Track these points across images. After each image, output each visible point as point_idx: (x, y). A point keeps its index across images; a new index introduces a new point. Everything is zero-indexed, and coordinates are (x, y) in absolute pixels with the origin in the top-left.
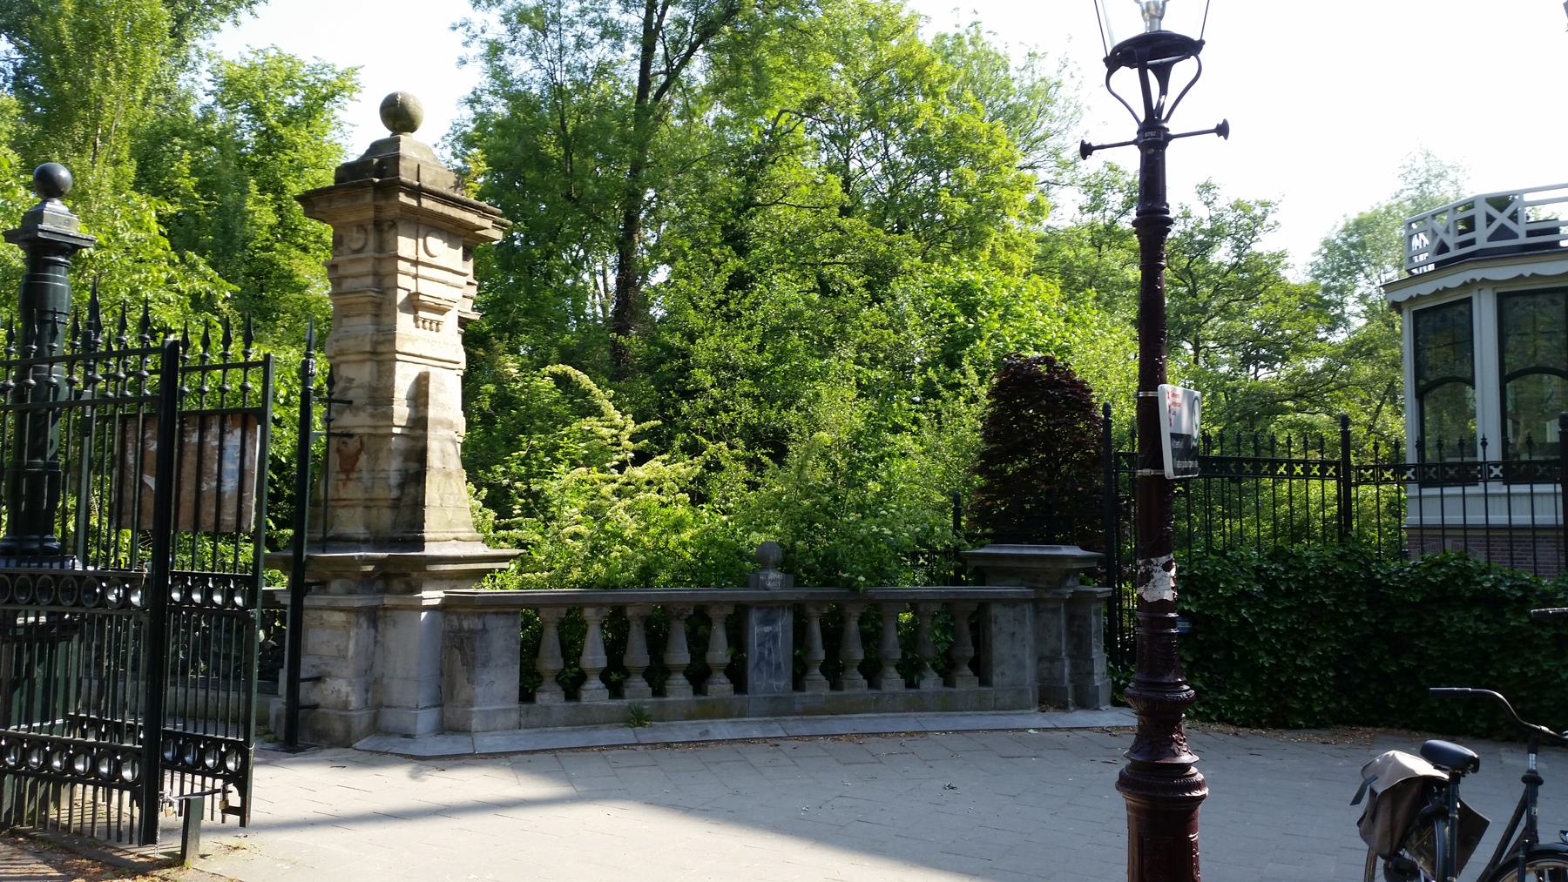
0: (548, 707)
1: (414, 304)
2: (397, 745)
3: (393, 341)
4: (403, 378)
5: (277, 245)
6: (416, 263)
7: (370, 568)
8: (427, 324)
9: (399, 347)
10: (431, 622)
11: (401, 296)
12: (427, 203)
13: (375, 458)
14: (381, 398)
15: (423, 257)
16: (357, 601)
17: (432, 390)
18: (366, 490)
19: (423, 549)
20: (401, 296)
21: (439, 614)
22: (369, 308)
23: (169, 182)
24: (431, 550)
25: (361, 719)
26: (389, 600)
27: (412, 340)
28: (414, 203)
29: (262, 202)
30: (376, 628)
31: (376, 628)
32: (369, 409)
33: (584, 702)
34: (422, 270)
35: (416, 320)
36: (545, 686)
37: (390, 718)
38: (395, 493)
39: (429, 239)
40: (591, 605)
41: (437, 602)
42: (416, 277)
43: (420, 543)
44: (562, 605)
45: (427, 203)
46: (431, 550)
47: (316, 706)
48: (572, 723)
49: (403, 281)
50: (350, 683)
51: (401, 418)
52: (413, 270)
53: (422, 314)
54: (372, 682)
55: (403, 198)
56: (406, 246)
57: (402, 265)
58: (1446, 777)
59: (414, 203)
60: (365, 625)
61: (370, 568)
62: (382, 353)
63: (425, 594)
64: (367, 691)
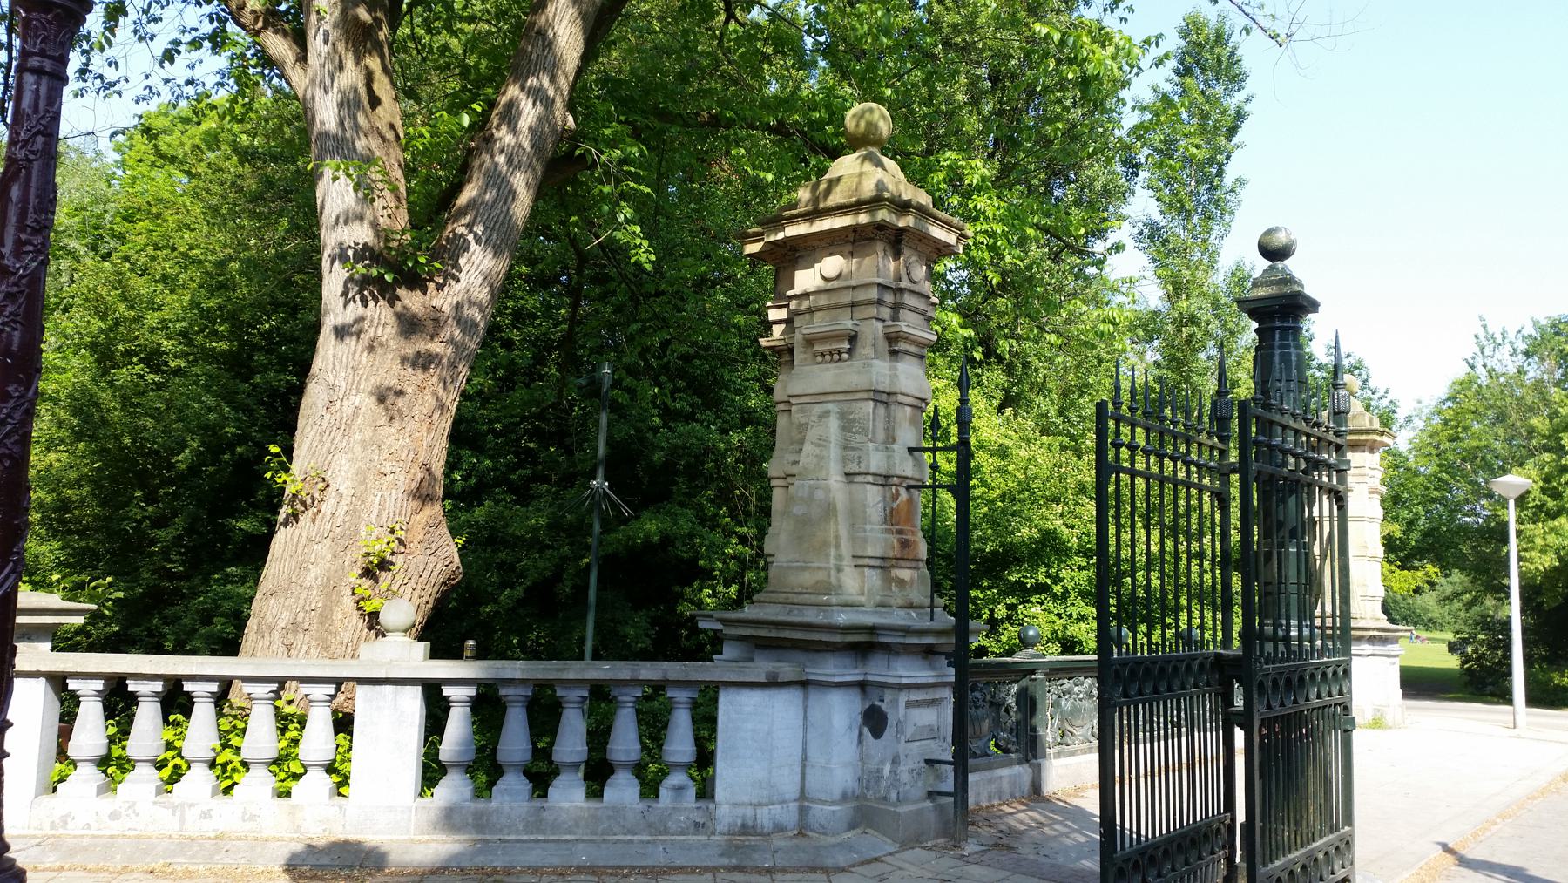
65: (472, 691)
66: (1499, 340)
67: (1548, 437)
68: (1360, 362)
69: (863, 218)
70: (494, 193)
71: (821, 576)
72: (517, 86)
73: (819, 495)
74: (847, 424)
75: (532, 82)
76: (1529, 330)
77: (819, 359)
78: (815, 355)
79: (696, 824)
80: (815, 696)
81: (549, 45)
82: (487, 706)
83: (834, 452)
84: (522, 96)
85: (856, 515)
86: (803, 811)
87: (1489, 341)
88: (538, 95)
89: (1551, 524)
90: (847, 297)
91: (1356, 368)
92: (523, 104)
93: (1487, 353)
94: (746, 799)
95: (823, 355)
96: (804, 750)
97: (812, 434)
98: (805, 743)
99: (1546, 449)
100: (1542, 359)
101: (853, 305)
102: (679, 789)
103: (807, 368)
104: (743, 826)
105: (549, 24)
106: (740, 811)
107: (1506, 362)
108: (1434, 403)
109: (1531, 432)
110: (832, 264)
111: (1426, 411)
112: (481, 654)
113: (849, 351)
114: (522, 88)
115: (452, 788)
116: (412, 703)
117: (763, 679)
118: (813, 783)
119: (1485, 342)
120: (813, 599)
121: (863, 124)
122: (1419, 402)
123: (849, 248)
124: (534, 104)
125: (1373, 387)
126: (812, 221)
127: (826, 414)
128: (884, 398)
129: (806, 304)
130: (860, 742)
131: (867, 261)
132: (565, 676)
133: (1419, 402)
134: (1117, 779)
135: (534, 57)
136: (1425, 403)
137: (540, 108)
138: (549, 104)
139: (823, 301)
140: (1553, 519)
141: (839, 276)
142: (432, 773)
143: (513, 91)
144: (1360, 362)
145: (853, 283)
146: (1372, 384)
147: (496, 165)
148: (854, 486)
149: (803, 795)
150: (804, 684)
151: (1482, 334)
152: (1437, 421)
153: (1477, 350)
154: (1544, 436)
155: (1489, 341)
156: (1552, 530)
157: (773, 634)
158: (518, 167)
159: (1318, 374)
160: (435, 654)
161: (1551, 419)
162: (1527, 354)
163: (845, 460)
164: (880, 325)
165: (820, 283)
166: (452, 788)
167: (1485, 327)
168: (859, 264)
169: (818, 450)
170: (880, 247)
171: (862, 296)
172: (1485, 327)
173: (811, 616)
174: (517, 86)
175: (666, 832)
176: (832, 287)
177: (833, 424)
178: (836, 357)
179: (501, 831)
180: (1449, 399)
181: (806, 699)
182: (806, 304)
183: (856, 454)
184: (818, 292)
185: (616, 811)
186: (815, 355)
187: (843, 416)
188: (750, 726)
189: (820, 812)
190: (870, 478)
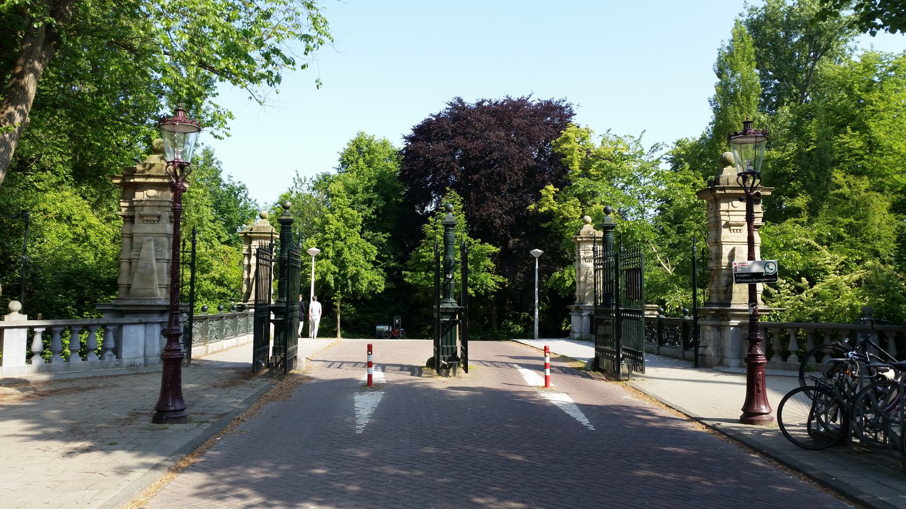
0: (775, 362)
1: (728, 225)
2: (727, 370)
3: (720, 238)
4: (726, 251)
5: (866, 157)
6: (728, 211)
7: (713, 312)
8: (735, 231)
9: (722, 240)
10: (735, 332)
11: (723, 223)
12: (727, 191)
13: (718, 276)
14: (719, 256)
15: (731, 208)
16: (715, 323)
17: (736, 253)
18: (716, 287)
19: (730, 306)
20: (723, 223)
21: (739, 329)
22: (714, 228)
23: (808, 135)
24: (733, 307)
25: (717, 360)
26: (723, 323)
27: (728, 237)
28: (723, 192)
29: (854, 136)
30: (720, 331)
31: (720, 331)
32: (715, 261)
33: (788, 362)
34: (731, 213)
35: (730, 230)
36: (774, 356)
37: (726, 361)
38: (725, 288)
39: (733, 202)
40: (789, 328)
41: (737, 324)
42: (729, 216)
43: (729, 305)
44: (778, 327)
45: (727, 191)
46: (733, 307)
47: (705, 355)
48: (783, 369)
49: (723, 218)
50: (712, 349)
51: (725, 263)
52: (727, 214)
53: (732, 228)
54: (720, 350)
55: (718, 192)
56: (724, 206)
57: (722, 213)
58: (378, 327)
59: (723, 192)
60: (716, 331)
61: (713, 312)
62: (718, 243)
63: (732, 321)
64: (718, 352)
65: (44, 329)
66: (303, 182)
67: (320, 226)
68: (244, 185)
69: (166, 181)
70: (4, 148)
71: (151, 291)
72: (13, 107)
73: (149, 266)
74: (157, 244)
75: (19, 107)
76: (315, 179)
77: (145, 222)
78: (144, 221)
79: (117, 365)
80: (149, 327)
81: (26, 93)
82: (48, 333)
83: (153, 252)
84: (16, 112)
85: (160, 272)
86: (146, 360)
87: (299, 181)
88: (21, 112)
89: (319, 262)
90: (158, 204)
91: (243, 189)
92: (16, 114)
93: (298, 186)
94: (131, 357)
95: (147, 221)
96: (145, 343)
97: (145, 246)
98: (145, 340)
99: (318, 230)
100: (319, 192)
101: (159, 206)
102: (110, 356)
103: (141, 225)
104: (131, 364)
105: (26, 85)
106: (130, 360)
107: (305, 190)
108: (272, 204)
109: (314, 223)
110: (152, 192)
111: (269, 208)
112: (45, 318)
113: (157, 221)
114: (15, 109)
115: (37, 361)
116: (24, 333)
117: (137, 322)
118: (148, 352)
119: (298, 182)
120: (149, 298)
121: (160, 147)
122: (266, 203)
123: (158, 188)
124: (20, 115)
125: (249, 198)
126: (147, 179)
127: (150, 240)
128: (168, 236)
129: (141, 204)
130: (160, 339)
131: (165, 193)
132: (76, 323)
133: (266, 203)
134: (734, 191)
135: (20, 97)
136: (268, 204)
137: (22, 117)
138: (25, 116)
139: (148, 204)
140: (320, 260)
141: (154, 197)
142: (29, 356)
143: (11, 109)
144: (244, 185)
145: (160, 199)
146: (249, 196)
147: (5, 138)
148: (159, 263)
149: (145, 355)
150: (145, 323)
151: (296, 178)
152: (273, 212)
153: (294, 185)
154: (319, 225)
155: (299, 181)
156: (319, 264)
157: (136, 309)
158: (13, 139)
159: (223, 188)
160: (29, 319)
161: (322, 218)
162: (314, 189)
163: (156, 255)
164: (168, 213)
165: (146, 197)
166: (37, 361)
167: (298, 175)
168: (162, 194)
169: (147, 252)
170: (169, 188)
171: (163, 204)
172: (298, 175)
173: (148, 303)
174: (13, 107)
175: (108, 368)
176: (150, 200)
177: (152, 243)
178: (152, 222)
179: (56, 371)
180: (278, 203)
181: (146, 328)
182: (141, 204)
183: (160, 253)
184: (147, 201)
185: (92, 363)
186: (144, 221)
187: (155, 241)
188: (132, 336)
189: (151, 360)
190: (165, 261)
